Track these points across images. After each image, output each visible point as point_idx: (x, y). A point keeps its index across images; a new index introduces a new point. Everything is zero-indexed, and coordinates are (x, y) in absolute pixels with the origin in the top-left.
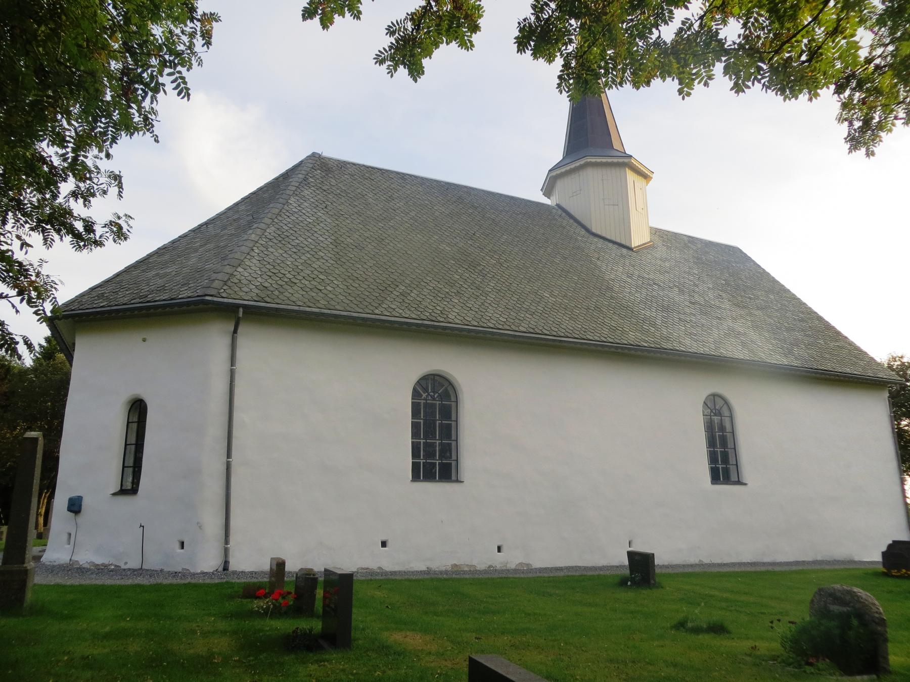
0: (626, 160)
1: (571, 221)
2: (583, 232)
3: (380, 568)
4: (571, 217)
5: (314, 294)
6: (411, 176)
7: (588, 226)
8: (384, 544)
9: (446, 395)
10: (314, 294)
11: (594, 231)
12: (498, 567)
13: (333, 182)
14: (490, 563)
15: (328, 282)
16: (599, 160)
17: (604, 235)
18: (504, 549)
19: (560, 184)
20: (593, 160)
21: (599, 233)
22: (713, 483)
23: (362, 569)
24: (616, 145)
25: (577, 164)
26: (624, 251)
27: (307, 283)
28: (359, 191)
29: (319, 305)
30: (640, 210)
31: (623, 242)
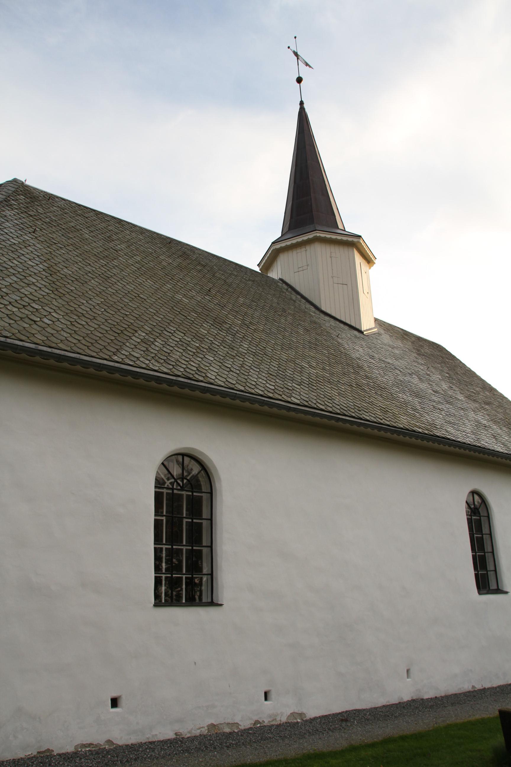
0: (355, 240)
1: (299, 297)
2: (313, 309)
3: (109, 742)
4: (298, 293)
5: (26, 325)
6: (129, 223)
8: (115, 703)
9: (194, 484)
10: (26, 325)
11: (323, 309)
12: (266, 723)
13: (41, 210)
14: (256, 718)
15: (45, 313)
16: (328, 236)
17: (333, 314)
18: (273, 695)
19: (283, 259)
22: (480, 594)
23: (84, 746)
24: (340, 227)
25: (299, 239)
26: (356, 333)
27: (15, 309)
28: (72, 224)
29: (36, 340)
31: (353, 324)
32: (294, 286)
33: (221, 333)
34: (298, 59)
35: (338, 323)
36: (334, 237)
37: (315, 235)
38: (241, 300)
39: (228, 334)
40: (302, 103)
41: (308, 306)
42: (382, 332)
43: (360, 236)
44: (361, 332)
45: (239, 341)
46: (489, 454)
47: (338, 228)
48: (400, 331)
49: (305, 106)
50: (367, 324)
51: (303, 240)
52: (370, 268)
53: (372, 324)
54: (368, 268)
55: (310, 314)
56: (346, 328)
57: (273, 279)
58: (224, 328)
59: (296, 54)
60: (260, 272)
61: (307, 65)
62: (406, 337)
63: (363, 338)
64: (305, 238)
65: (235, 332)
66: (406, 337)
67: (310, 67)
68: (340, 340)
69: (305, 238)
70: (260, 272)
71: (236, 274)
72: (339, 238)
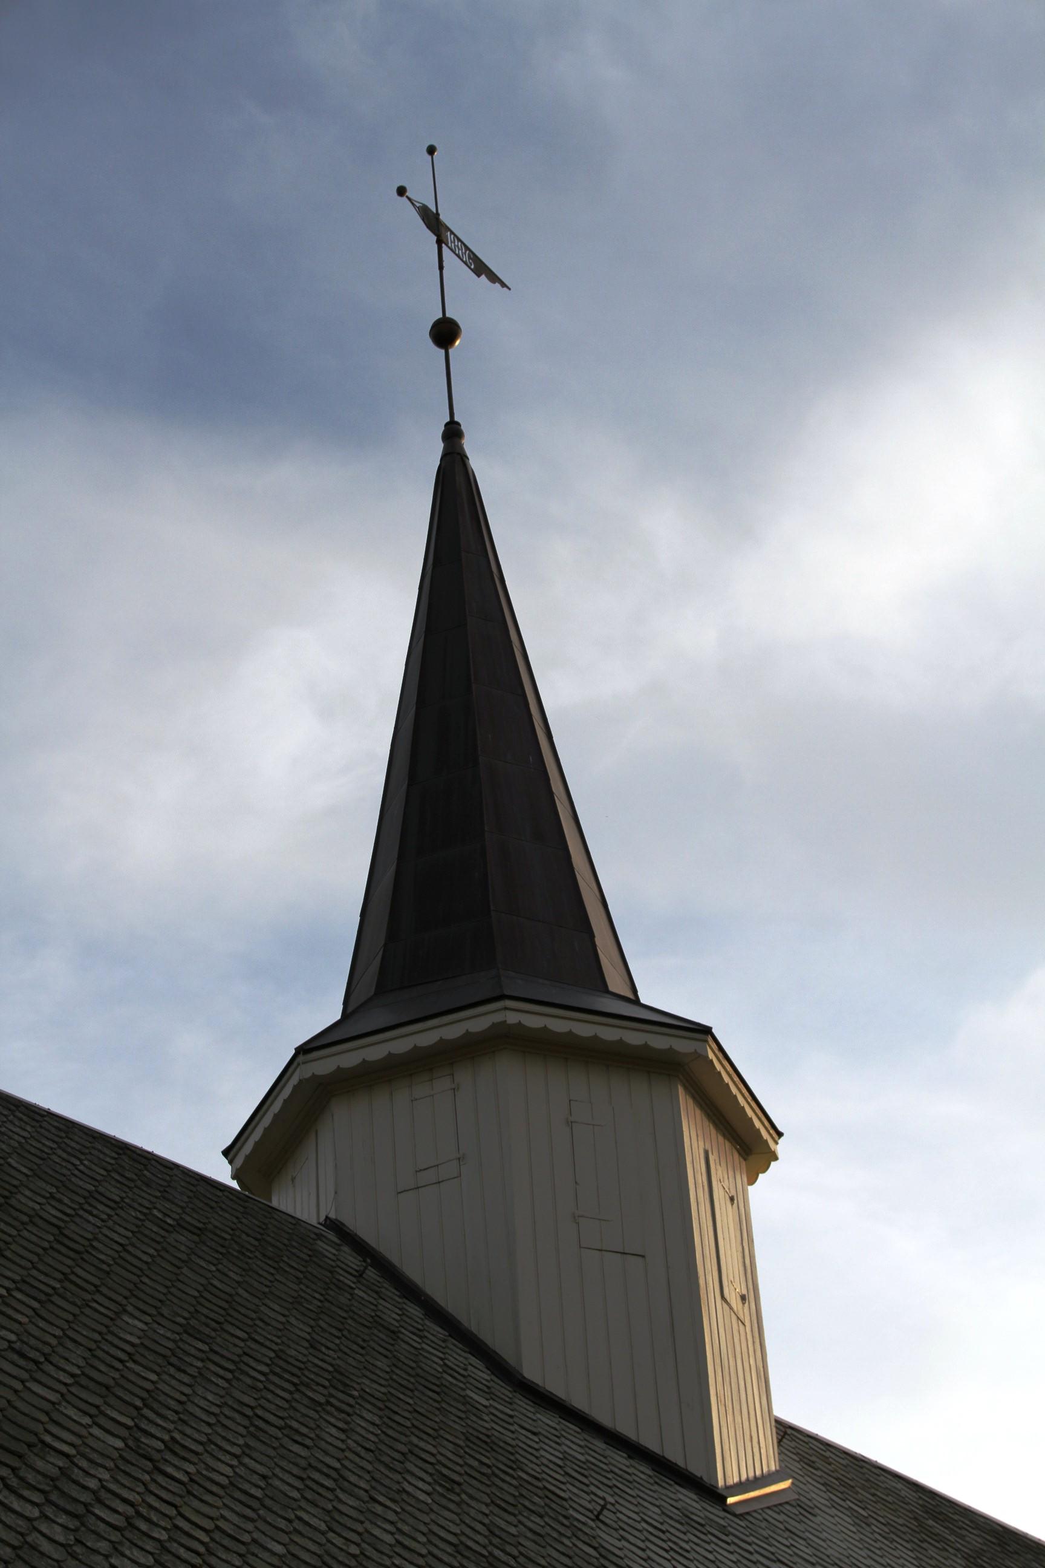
0: (683, 1046)
1: (415, 1311)
4: (410, 1291)
7: (498, 1342)
11: (531, 1372)
17: (578, 1401)
19: (346, 1125)
20: (533, 1022)
21: (555, 1387)
24: (616, 984)
25: (426, 1036)
26: (687, 1498)
30: (735, 1301)
31: (674, 1455)
32: (394, 1258)
33: (16, 1505)
34: (440, 242)
35: (599, 1445)
36: (584, 1029)
37: (497, 1018)
38: (133, 1326)
39: (49, 1511)
40: (452, 433)
41: (458, 1356)
42: (818, 1496)
43: (707, 1031)
44: (715, 1496)
45: (103, 1546)
46: (139, 1155)
47: (605, 989)
48: (905, 1492)
49: (469, 445)
50: (740, 1458)
51: (545, 1029)
52: (752, 1181)
53: (765, 1456)
54: (741, 1178)
55: (465, 1400)
56: (642, 1471)
57: (298, 1221)
58: (31, 1477)
59: (432, 221)
60: (234, 1184)
61: (480, 268)
62: (938, 1528)
63: (723, 1529)
64: (452, 1029)
65: (85, 1497)
66: (938, 1528)
67: (493, 278)
68: (608, 1539)
69: (452, 1029)
70: (234, 1184)
71: (114, 1193)
72: (609, 1034)
